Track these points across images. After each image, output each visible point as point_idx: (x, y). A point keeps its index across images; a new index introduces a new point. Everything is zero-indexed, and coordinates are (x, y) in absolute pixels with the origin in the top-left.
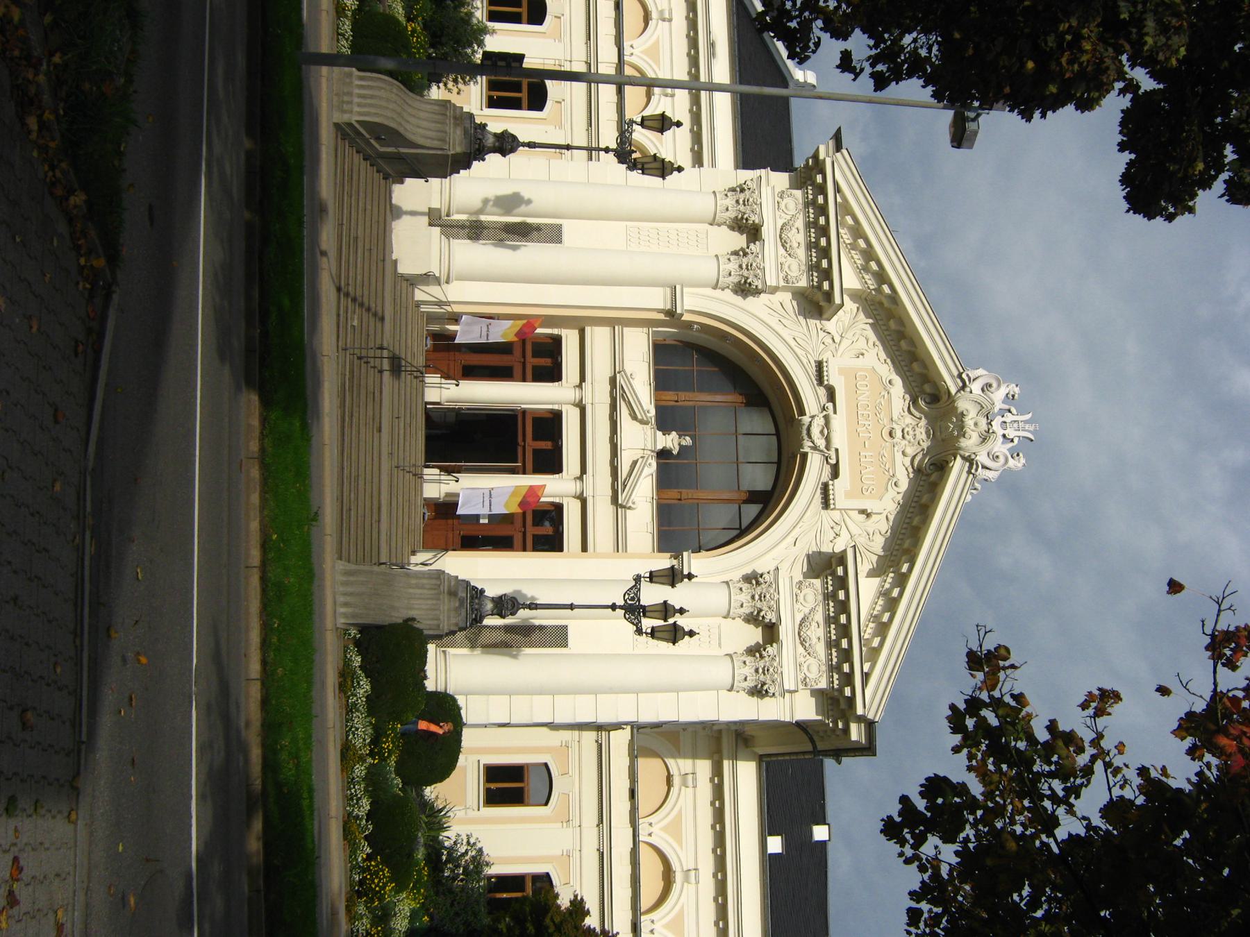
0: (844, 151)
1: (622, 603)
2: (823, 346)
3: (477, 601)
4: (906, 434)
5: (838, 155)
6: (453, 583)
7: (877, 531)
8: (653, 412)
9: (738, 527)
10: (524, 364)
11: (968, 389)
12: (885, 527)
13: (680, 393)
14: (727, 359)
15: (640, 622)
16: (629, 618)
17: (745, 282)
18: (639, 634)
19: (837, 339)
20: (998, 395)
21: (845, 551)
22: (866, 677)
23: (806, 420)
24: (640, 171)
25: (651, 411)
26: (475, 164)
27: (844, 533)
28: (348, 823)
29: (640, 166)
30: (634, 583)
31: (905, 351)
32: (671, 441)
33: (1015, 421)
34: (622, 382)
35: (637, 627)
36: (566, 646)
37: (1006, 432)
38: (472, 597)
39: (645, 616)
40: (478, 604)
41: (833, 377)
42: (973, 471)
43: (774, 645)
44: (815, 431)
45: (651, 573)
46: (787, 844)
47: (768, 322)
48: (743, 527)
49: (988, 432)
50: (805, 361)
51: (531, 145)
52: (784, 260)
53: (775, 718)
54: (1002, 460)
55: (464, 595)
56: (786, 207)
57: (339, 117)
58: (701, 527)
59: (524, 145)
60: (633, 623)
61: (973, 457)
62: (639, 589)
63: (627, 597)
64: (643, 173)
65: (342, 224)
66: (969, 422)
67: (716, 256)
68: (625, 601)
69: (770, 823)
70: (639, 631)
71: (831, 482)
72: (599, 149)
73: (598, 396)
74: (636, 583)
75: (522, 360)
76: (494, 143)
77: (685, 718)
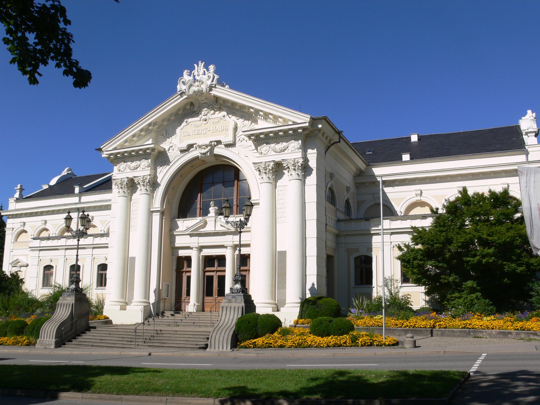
0: (101, 147)
5: (103, 149)
10: (217, 271)
11: (184, 91)
17: (272, 170)
19: (171, 145)
22: (295, 123)
23: (199, 155)
28: (392, 352)
31: (175, 117)
32: (212, 210)
33: (198, 71)
34: (189, 231)
36: (285, 252)
37: (201, 74)
41: (184, 146)
42: (214, 86)
43: (282, 162)
44: (204, 151)
46: (405, 152)
47: (165, 173)
50: (179, 157)
52: (141, 168)
53: (315, 160)
55: (231, 296)
56: (123, 168)
57: (53, 346)
61: (208, 86)
65: (92, 345)
66: (196, 89)
67: (289, 181)
69: (396, 159)
71: (223, 143)
72: (78, 245)
73: (195, 242)
75: (215, 272)
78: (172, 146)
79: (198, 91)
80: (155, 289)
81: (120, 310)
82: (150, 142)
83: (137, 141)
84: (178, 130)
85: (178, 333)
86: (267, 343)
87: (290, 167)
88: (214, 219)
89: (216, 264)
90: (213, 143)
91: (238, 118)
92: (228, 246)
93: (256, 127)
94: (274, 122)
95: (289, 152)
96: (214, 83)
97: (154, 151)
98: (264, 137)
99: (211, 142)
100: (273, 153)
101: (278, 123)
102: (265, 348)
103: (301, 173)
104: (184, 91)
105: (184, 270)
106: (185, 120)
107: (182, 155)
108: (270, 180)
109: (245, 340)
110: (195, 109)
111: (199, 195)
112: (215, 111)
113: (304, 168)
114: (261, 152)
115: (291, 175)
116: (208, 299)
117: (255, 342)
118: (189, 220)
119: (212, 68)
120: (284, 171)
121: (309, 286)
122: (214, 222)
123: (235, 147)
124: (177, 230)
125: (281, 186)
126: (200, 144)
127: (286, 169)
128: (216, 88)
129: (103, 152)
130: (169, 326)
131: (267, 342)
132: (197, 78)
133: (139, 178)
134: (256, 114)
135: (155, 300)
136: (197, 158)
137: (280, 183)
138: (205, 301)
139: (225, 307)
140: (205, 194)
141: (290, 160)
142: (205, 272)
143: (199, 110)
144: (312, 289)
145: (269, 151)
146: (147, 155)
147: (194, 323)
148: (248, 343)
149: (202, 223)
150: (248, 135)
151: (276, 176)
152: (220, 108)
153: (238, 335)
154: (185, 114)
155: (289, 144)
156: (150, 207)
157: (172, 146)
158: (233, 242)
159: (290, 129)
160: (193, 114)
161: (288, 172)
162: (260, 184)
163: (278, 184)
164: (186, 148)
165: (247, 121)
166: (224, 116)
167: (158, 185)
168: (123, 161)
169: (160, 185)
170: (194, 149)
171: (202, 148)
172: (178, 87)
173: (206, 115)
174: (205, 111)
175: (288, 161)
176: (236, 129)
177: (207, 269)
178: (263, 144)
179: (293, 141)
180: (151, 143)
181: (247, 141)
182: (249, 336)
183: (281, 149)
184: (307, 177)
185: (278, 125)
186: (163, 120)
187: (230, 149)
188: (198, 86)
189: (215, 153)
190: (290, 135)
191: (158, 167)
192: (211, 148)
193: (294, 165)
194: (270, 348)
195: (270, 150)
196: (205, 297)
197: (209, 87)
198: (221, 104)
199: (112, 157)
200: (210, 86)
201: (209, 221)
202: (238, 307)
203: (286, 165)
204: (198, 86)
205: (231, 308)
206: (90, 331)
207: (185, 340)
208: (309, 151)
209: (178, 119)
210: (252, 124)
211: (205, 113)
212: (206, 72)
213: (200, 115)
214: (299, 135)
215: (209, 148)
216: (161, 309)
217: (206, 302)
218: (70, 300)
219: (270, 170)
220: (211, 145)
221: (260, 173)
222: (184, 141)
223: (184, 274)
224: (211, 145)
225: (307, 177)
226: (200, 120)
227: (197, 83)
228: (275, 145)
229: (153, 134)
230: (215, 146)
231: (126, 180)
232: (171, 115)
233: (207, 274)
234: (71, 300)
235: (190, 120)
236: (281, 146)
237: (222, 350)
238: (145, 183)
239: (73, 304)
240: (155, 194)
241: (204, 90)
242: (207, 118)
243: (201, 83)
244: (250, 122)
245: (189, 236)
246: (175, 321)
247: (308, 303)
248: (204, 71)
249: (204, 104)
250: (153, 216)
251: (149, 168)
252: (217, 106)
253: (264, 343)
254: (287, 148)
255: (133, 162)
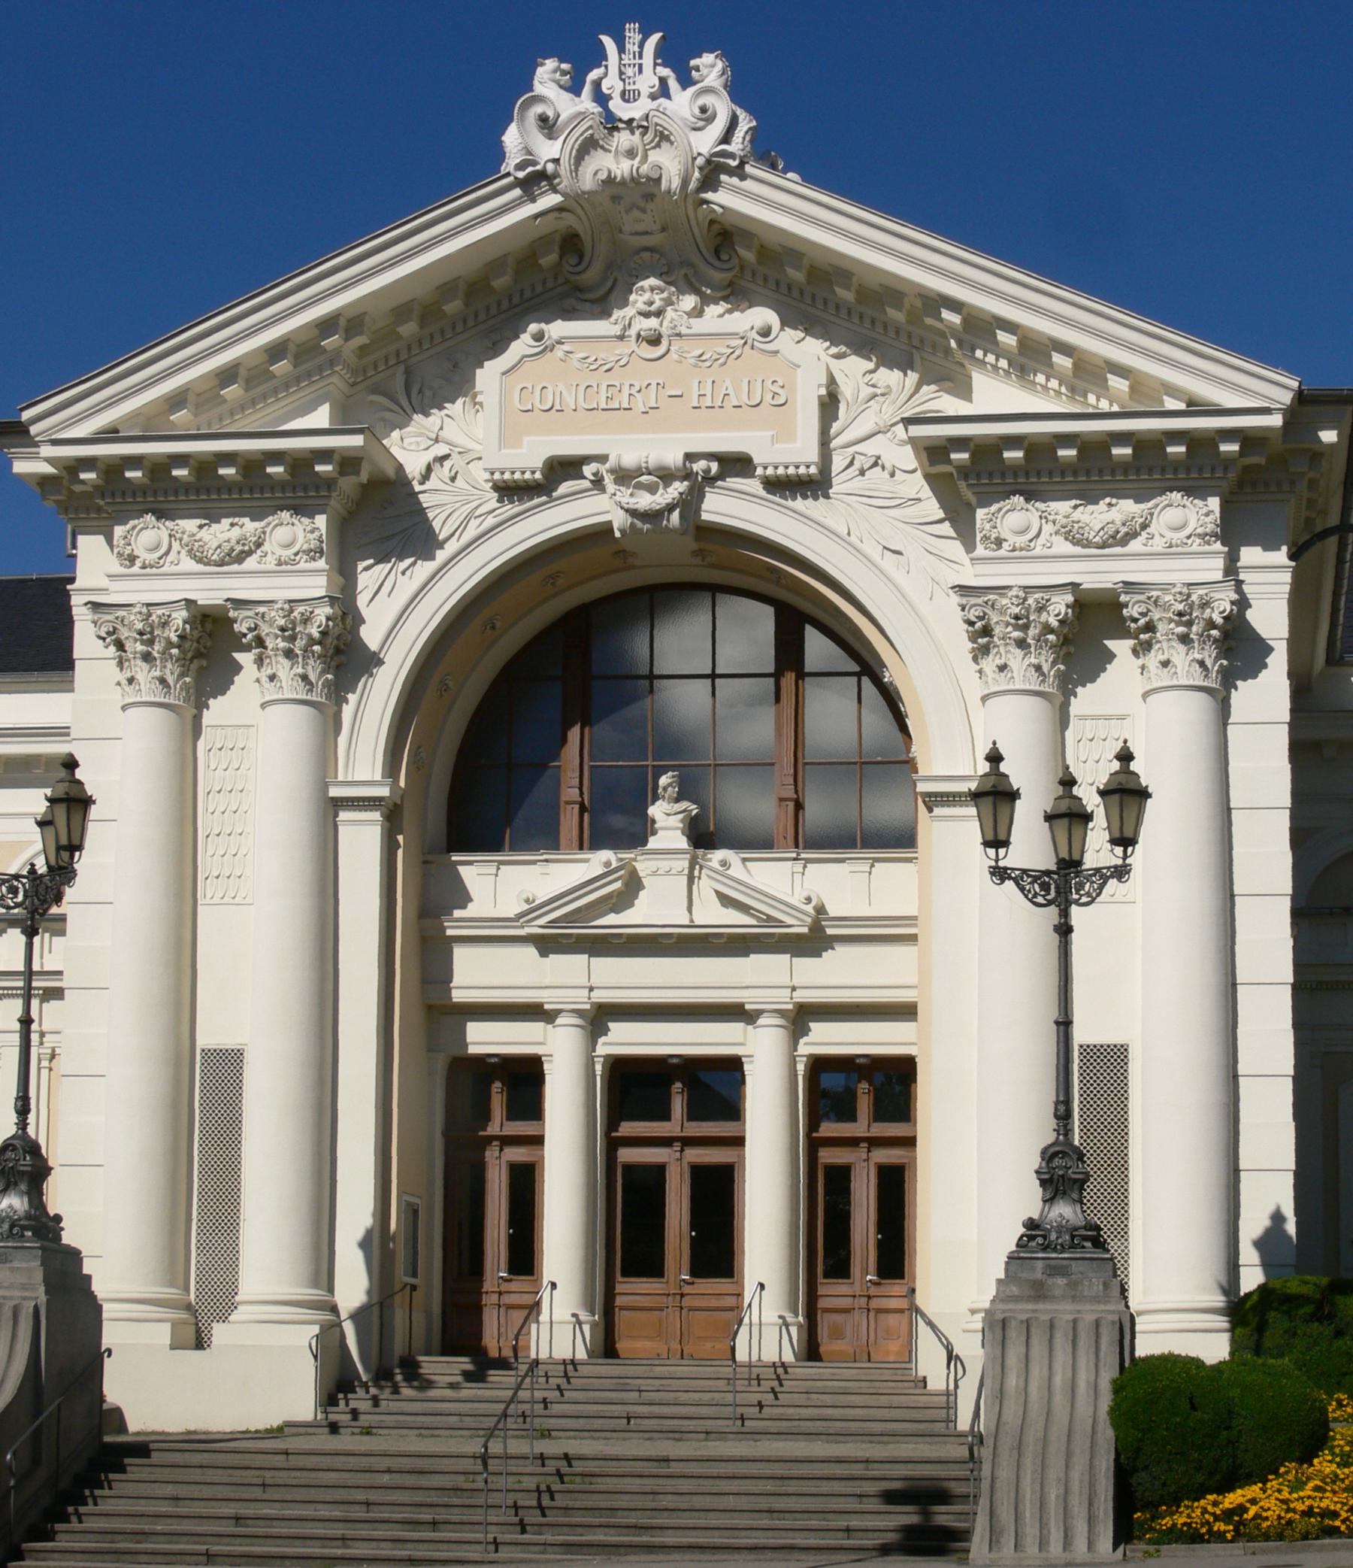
0: (26, 415)
1: (1053, 911)
2: (459, 482)
3: (1053, 1236)
4: (653, 308)
5: (34, 430)
6: (1014, 1290)
7: (868, 377)
8: (606, 855)
9: (855, 679)
10: (688, 1142)
11: (550, 167)
12: (856, 365)
13: (563, 798)
14: (483, 698)
15: (1097, 870)
16: (1088, 894)
17: (319, 643)
18: (1128, 872)
19: (441, 450)
20: (564, 105)
21: (913, 441)
22: (1196, 407)
23: (619, 520)
24: (77, 854)
25: (604, 859)
26: (69, 1237)
27: (870, 448)
29: (65, 855)
30: (1009, 884)
31: (466, 305)
33: (621, 73)
35: (1112, 876)
37: (645, 91)
38: (1045, 1248)
39: (1080, 863)
40: (1059, 1233)
42: (734, 163)
44: (645, 501)
45: (987, 844)
48: (857, 669)
49: (646, 128)
50: (490, 521)
51: (23, 1108)
54: (708, 100)
55: (1040, 1264)
58: (857, 759)
59: (23, 1124)
60: (1101, 887)
61: (700, 161)
62: (1024, 871)
63: (1040, 900)
64: (80, 847)
65: (207, 1554)
66: (623, 168)
68: (1049, 903)
70: (1121, 872)
71: (759, 471)
74: (1010, 878)
75: (677, 1146)
76: (21, 1194)
77: (1283, 796)
78: (446, 457)
79: (635, 180)
80: (369, 1233)
81: (173, 1347)
82: (321, 417)
83: (243, 408)
84: (488, 375)
85: (675, 1468)
86: (1309, 1513)
87: (270, 643)
88: (686, 864)
89: (678, 1106)
90: (699, 466)
91: (843, 348)
92: (559, 1011)
93: (949, 404)
94: (1072, 389)
95: (1155, 549)
96: (736, 146)
97: (357, 473)
98: (146, 481)
99: (690, 457)
100: (189, 565)
101: (1092, 398)
102: (1305, 1537)
103: (323, 672)
104: (550, 167)
105: (494, 1128)
106: (533, 327)
107: (510, 509)
108: (311, 690)
109: (1175, 1502)
110: (591, 276)
111: (574, 734)
112: (706, 300)
113: (338, 651)
114: (127, 552)
115: (272, 678)
116: (633, 1290)
117: (1241, 1509)
118: (534, 862)
119: (710, 67)
120: (237, 656)
121: (1253, 1224)
122: (684, 880)
123: (827, 497)
124: (458, 913)
125: (1094, 718)
126: (629, 460)
127: (247, 648)
128: (743, 177)
129: (36, 445)
130: (368, 1433)
131: (1311, 1507)
132: (617, 106)
133: (121, 613)
134: (968, 337)
135: (369, 1293)
136: (601, 533)
137: (217, 710)
138: (619, 1301)
139: (1013, 1323)
140: (604, 730)
141: (1166, 587)
142: (613, 1144)
143: (609, 284)
144: (1270, 1243)
145: (1038, 536)
146: (991, 476)
147: (629, 1419)
148: (1205, 1511)
149: (618, 885)
150: (928, 443)
151: (201, 676)
152: (731, 284)
153: (1135, 1470)
154: (528, 294)
155: (268, 530)
156: (325, 777)
157: (446, 457)
158: (591, 989)
159: (1175, 436)
160: (570, 302)
161: (260, 661)
162: (985, 699)
163: (208, 718)
164: (538, 476)
165: (897, 374)
166: (765, 332)
167: (372, 661)
168: (154, 512)
169: (380, 662)
170: (586, 484)
171: (640, 486)
172: (511, 138)
173: (659, 313)
174: (647, 291)
175: (1154, 593)
176: (829, 405)
177: (627, 1129)
178: (1007, 496)
179: (285, 515)
180: (325, 424)
181: (892, 475)
182: (1200, 1478)
183: (226, 547)
184: (1239, 683)
185: (1091, 410)
186: (402, 312)
187: (799, 504)
188: (631, 154)
189: (705, 516)
190: (273, 484)
191: (361, 566)
192: (691, 489)
193: (289, 632)
194: (1327, 1541)
195: (1048, 528)
196: (619, 1278)
197: (701, 169)
198: (742, 268)
199: (83, 482)
200: (708, 162)
201: (655, 873)
202: (1097, 1324)
203: (250, 629)
204: (631, 154)
205: (1052, 1326)
206: (122, 1469)
207: (764, 1506)
208: (1250, 555)
209: (482, 316)
210: (925, 388)
211: (651, 303)
212: (673, 84)
213: (617, 314)
214: (1213, 469)
215: (678, 488)
216: (399, 1348)
217: (622, 1308)
218: (10, 1287)
219: (312, 641)
220: (688, 475)
221: (120, 657)
222: (526, 440)
223: (491, 1154)
224: (688, 475)
225: (1239, 683)
226: (621, 338)
227: (624, 139)
228: (1075, 507)
229: (336, 381)
230: (710, 480)
231: (184, 614)
232: (447, 290)
233: (627, 1155)
234: (24, 1287)
235: (558, 328)
236: (226, 536)
237: (1068, 1556)
238: (300, 643)
239: (36, 1309)
240: (347, 711)
241: (672, 180)
242: (665, 331)
243: (648, 137)
244: (913, 377)
245: (531, 951)
246: (740, 1410)
247: (1288, 1313)
248: (663, 81)
249: (646, 255)
250: (341, 829)
251: (322, 564)
252: (718, 276)
253: (1294, 1511)
254: (259, 545)
255: (215, 519)
